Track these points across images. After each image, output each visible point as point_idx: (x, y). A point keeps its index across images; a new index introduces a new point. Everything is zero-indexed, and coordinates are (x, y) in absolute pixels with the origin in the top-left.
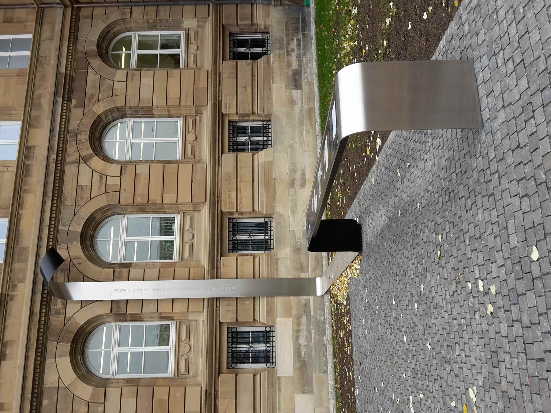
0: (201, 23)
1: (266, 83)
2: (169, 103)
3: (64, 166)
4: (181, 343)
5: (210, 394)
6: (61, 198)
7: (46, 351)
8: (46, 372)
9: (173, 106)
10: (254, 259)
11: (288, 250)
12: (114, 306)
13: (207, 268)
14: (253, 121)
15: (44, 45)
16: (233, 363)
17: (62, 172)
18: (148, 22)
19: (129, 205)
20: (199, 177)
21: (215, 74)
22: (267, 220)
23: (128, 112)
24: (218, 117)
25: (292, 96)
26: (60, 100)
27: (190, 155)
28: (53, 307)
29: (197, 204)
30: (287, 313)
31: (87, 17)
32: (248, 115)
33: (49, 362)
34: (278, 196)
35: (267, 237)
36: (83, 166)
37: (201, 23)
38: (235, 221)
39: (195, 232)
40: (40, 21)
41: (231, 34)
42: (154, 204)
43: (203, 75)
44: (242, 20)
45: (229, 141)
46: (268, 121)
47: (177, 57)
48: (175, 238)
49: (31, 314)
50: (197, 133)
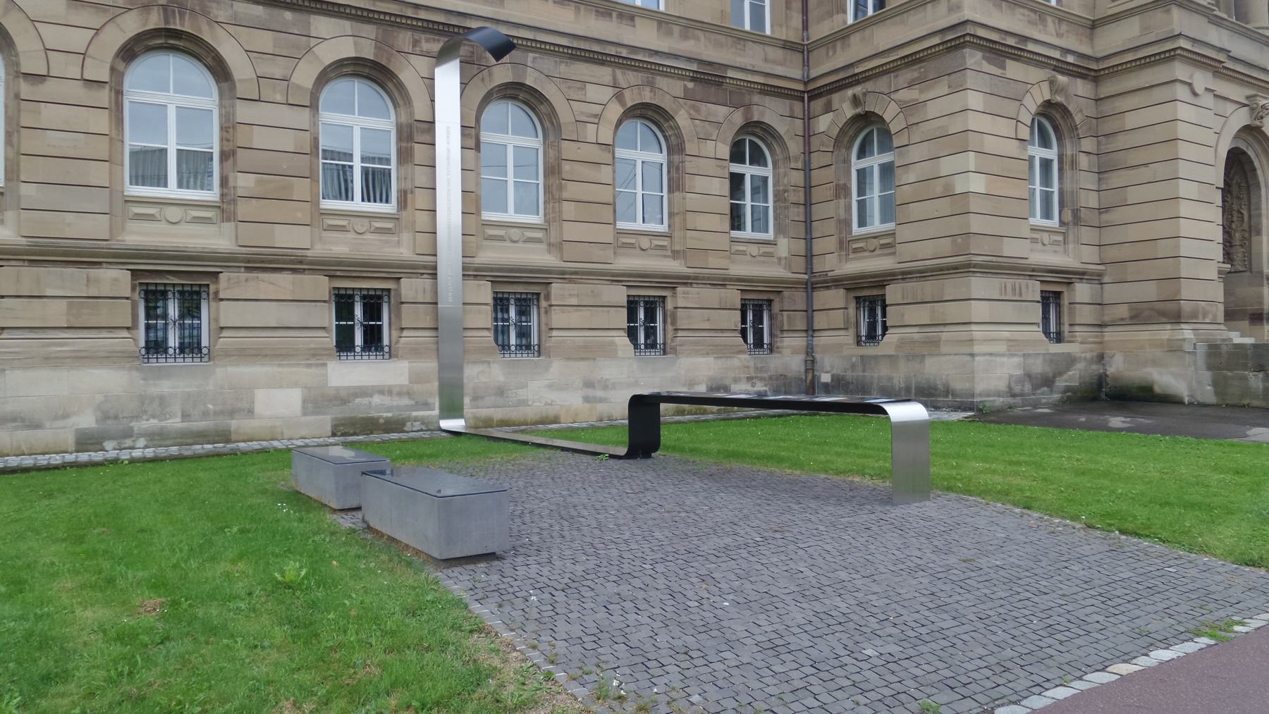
0: (783, 262)
2: (689, 215)
4: (366, 220)
5: (301, 262)
7: (363, 22)
8: (333, 20)
9: (685, 220)
10: (128, 328)
11: (501, 378)
12: (425, 126)
13: (476, 260)
14: (664, 330)
15: (758, 48)
17: (602, 63)
18: (785, 191)
19: (559, 152)
20: (597, 253)
21: (725, 279)
22: (386, 349)
23: (676, 158)
24: (673, 282)
26: (694, 67)
27: (625, 240)
28: (423, 36)
29: (561, 250)
30: (416, 378)
31: (792, 110)
32: (673, 323)
33: (347, 26)
34: (572, 363)
35: (358, 349)
36: (610, 92)
37: (783, 262)
38: (386, 299)
39: (520, 245)
40: (787, 46)
41: (770, 302)
42: (560, 188)
43: (723, 263)
44: (789, 316)
46: (390, 352)
47: (162, 181)
48: (172, 191)
50: (650, 252)
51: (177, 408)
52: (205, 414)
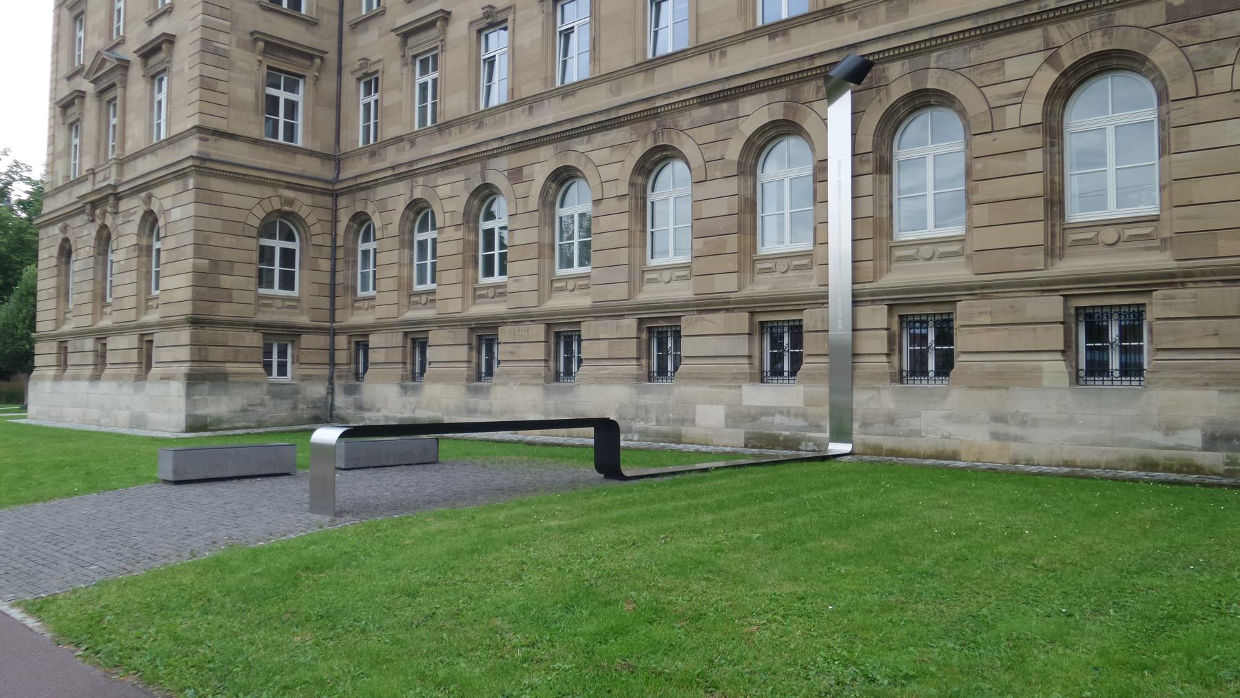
1: (1220, 376)
3: (1040, 26)
5: (729, 303)
6: (983, 39)
11: (892, 406)
16: (1120, 314)
17: (1029, 27)
20: (1020, 259)
25: (1188, 428)
30: (810, 401)
33: (764, 97)
35: (931, 374)
45: (1093, 307)
49: (812, 57)
51: (653, 416)
52: (668, 421)
